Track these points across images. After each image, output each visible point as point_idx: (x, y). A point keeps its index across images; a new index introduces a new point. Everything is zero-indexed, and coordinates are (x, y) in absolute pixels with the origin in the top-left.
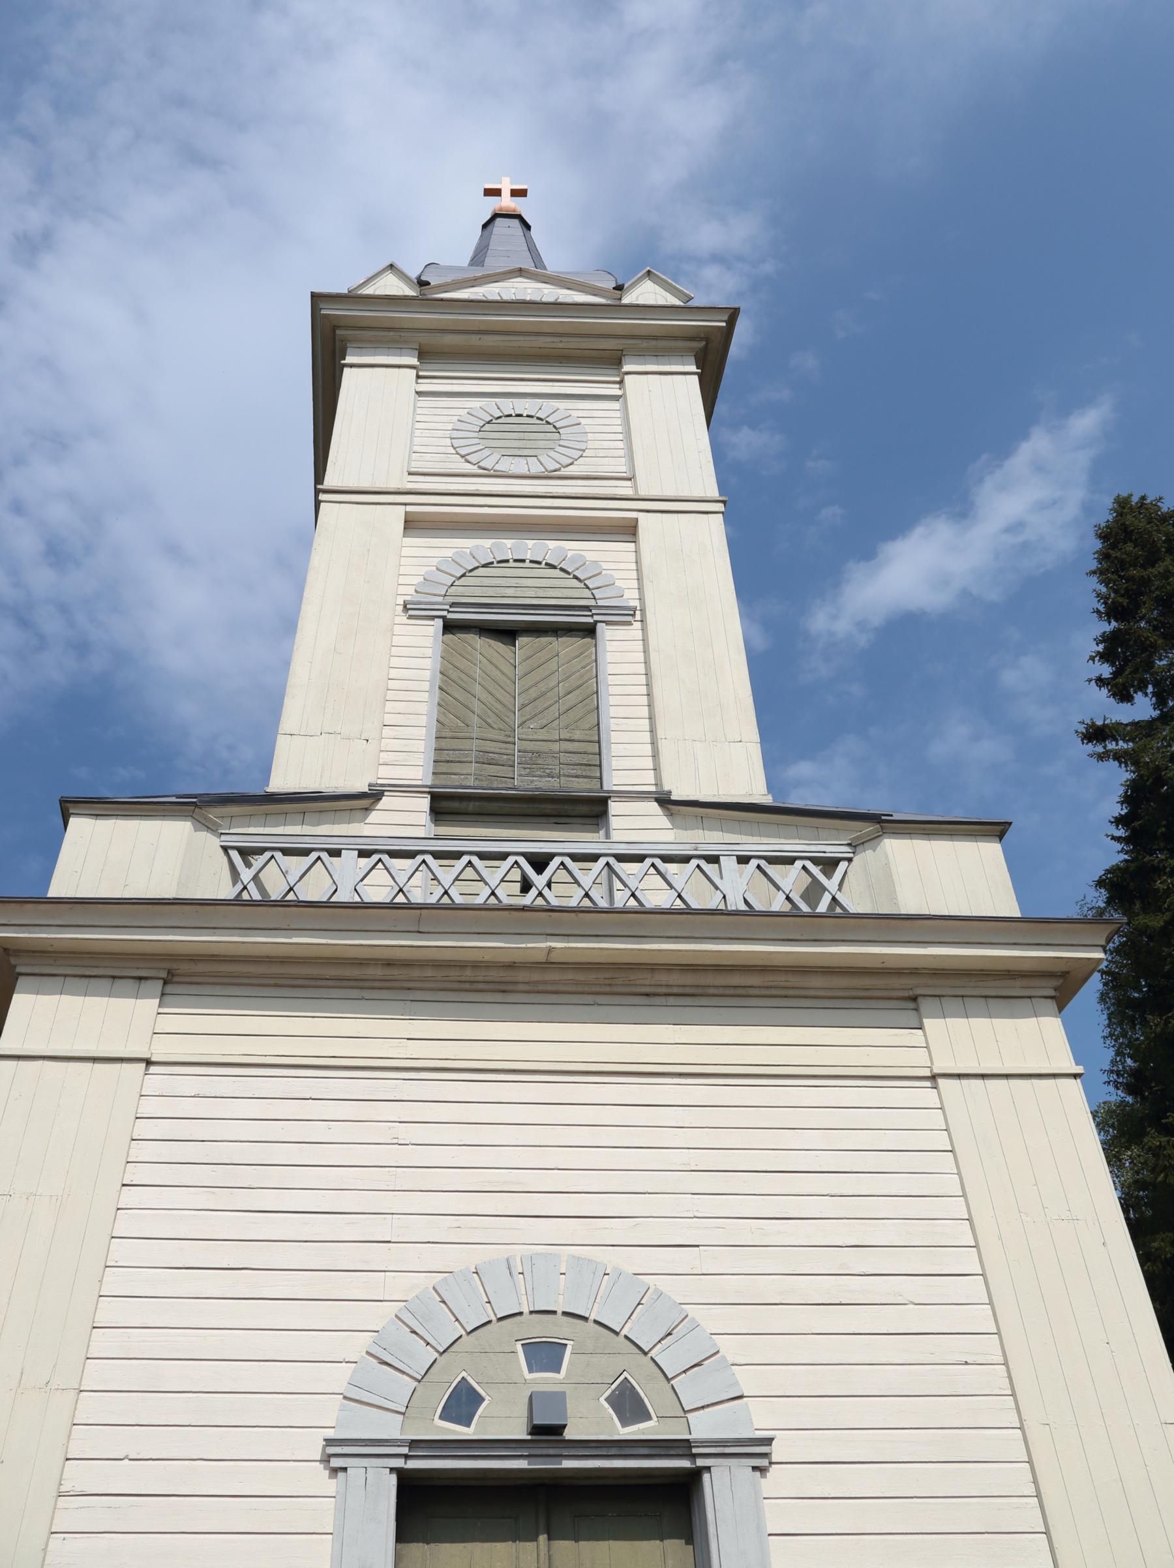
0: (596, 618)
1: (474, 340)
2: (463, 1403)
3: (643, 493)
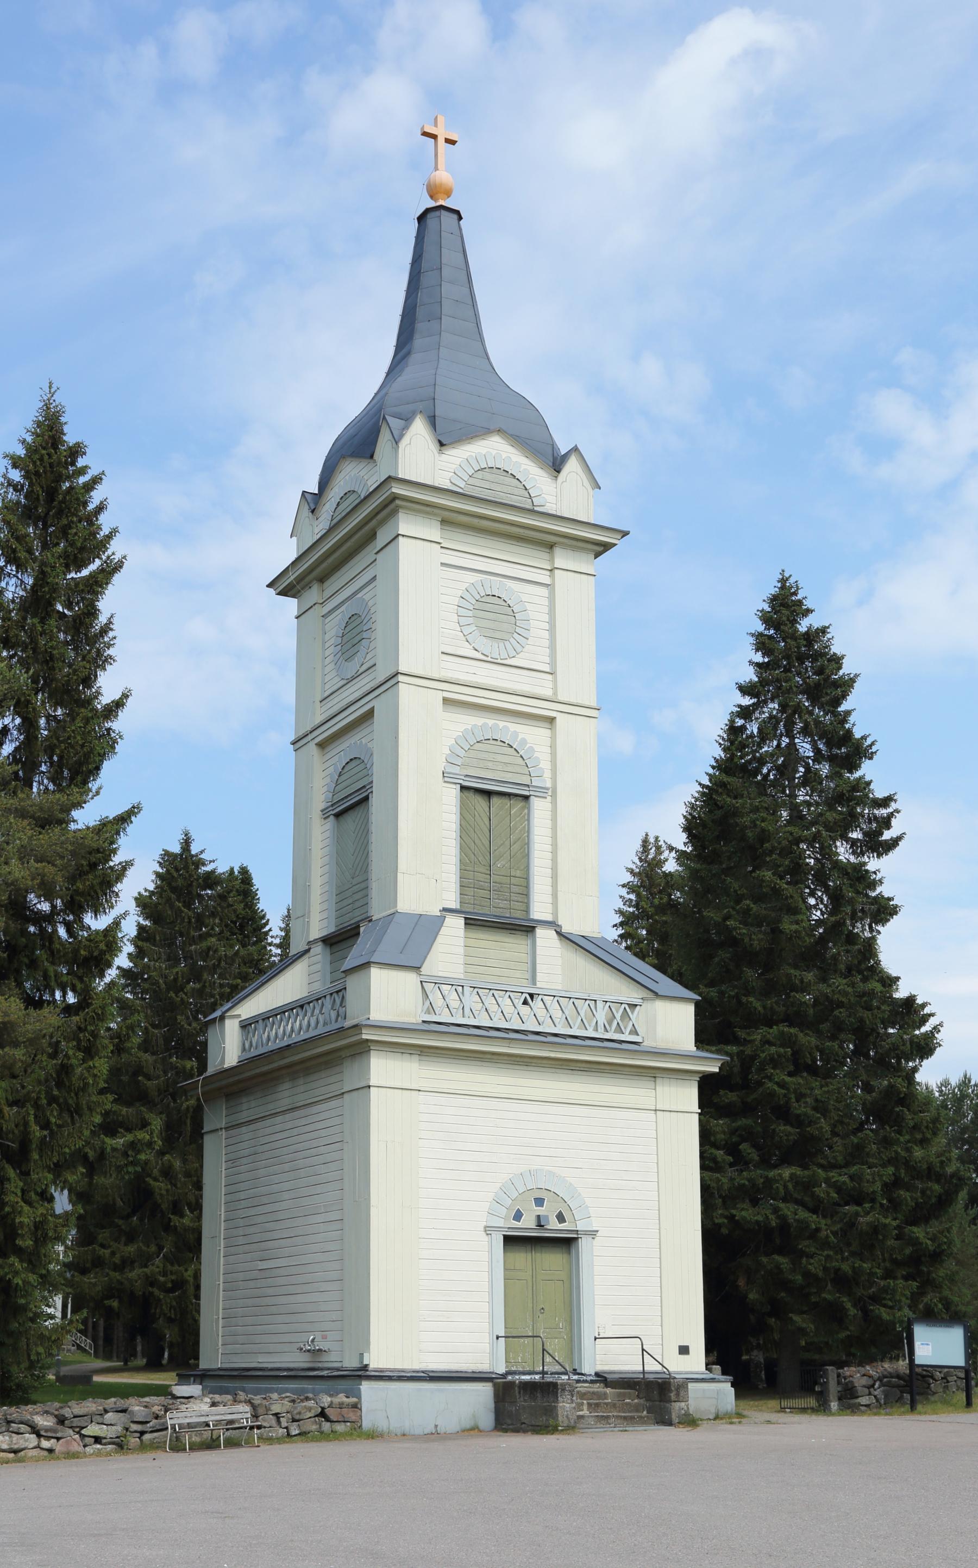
0: (532, 793)
1: (475, 521)
2: (518, 1216)
3: (560, 698)
